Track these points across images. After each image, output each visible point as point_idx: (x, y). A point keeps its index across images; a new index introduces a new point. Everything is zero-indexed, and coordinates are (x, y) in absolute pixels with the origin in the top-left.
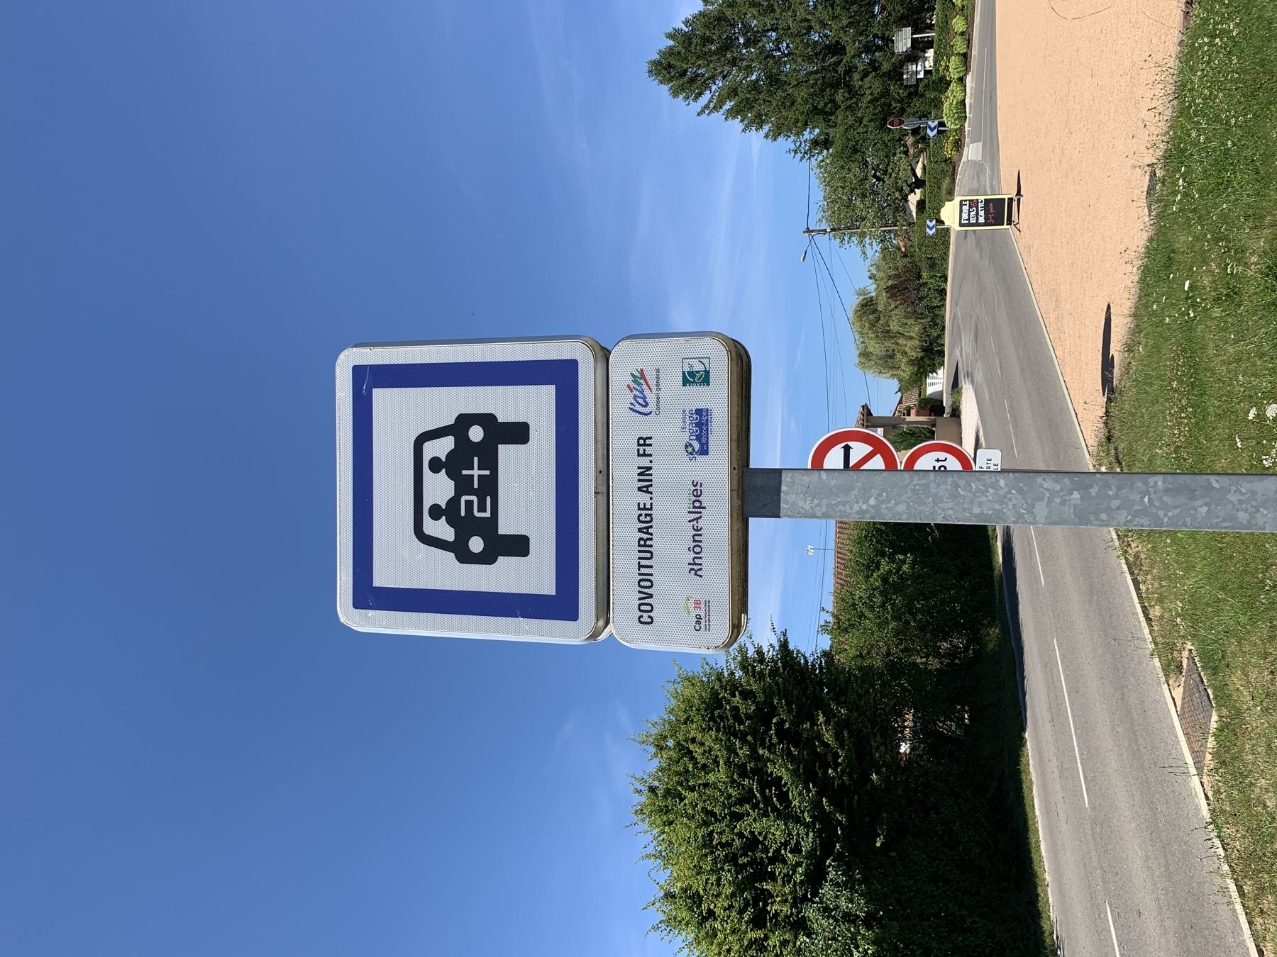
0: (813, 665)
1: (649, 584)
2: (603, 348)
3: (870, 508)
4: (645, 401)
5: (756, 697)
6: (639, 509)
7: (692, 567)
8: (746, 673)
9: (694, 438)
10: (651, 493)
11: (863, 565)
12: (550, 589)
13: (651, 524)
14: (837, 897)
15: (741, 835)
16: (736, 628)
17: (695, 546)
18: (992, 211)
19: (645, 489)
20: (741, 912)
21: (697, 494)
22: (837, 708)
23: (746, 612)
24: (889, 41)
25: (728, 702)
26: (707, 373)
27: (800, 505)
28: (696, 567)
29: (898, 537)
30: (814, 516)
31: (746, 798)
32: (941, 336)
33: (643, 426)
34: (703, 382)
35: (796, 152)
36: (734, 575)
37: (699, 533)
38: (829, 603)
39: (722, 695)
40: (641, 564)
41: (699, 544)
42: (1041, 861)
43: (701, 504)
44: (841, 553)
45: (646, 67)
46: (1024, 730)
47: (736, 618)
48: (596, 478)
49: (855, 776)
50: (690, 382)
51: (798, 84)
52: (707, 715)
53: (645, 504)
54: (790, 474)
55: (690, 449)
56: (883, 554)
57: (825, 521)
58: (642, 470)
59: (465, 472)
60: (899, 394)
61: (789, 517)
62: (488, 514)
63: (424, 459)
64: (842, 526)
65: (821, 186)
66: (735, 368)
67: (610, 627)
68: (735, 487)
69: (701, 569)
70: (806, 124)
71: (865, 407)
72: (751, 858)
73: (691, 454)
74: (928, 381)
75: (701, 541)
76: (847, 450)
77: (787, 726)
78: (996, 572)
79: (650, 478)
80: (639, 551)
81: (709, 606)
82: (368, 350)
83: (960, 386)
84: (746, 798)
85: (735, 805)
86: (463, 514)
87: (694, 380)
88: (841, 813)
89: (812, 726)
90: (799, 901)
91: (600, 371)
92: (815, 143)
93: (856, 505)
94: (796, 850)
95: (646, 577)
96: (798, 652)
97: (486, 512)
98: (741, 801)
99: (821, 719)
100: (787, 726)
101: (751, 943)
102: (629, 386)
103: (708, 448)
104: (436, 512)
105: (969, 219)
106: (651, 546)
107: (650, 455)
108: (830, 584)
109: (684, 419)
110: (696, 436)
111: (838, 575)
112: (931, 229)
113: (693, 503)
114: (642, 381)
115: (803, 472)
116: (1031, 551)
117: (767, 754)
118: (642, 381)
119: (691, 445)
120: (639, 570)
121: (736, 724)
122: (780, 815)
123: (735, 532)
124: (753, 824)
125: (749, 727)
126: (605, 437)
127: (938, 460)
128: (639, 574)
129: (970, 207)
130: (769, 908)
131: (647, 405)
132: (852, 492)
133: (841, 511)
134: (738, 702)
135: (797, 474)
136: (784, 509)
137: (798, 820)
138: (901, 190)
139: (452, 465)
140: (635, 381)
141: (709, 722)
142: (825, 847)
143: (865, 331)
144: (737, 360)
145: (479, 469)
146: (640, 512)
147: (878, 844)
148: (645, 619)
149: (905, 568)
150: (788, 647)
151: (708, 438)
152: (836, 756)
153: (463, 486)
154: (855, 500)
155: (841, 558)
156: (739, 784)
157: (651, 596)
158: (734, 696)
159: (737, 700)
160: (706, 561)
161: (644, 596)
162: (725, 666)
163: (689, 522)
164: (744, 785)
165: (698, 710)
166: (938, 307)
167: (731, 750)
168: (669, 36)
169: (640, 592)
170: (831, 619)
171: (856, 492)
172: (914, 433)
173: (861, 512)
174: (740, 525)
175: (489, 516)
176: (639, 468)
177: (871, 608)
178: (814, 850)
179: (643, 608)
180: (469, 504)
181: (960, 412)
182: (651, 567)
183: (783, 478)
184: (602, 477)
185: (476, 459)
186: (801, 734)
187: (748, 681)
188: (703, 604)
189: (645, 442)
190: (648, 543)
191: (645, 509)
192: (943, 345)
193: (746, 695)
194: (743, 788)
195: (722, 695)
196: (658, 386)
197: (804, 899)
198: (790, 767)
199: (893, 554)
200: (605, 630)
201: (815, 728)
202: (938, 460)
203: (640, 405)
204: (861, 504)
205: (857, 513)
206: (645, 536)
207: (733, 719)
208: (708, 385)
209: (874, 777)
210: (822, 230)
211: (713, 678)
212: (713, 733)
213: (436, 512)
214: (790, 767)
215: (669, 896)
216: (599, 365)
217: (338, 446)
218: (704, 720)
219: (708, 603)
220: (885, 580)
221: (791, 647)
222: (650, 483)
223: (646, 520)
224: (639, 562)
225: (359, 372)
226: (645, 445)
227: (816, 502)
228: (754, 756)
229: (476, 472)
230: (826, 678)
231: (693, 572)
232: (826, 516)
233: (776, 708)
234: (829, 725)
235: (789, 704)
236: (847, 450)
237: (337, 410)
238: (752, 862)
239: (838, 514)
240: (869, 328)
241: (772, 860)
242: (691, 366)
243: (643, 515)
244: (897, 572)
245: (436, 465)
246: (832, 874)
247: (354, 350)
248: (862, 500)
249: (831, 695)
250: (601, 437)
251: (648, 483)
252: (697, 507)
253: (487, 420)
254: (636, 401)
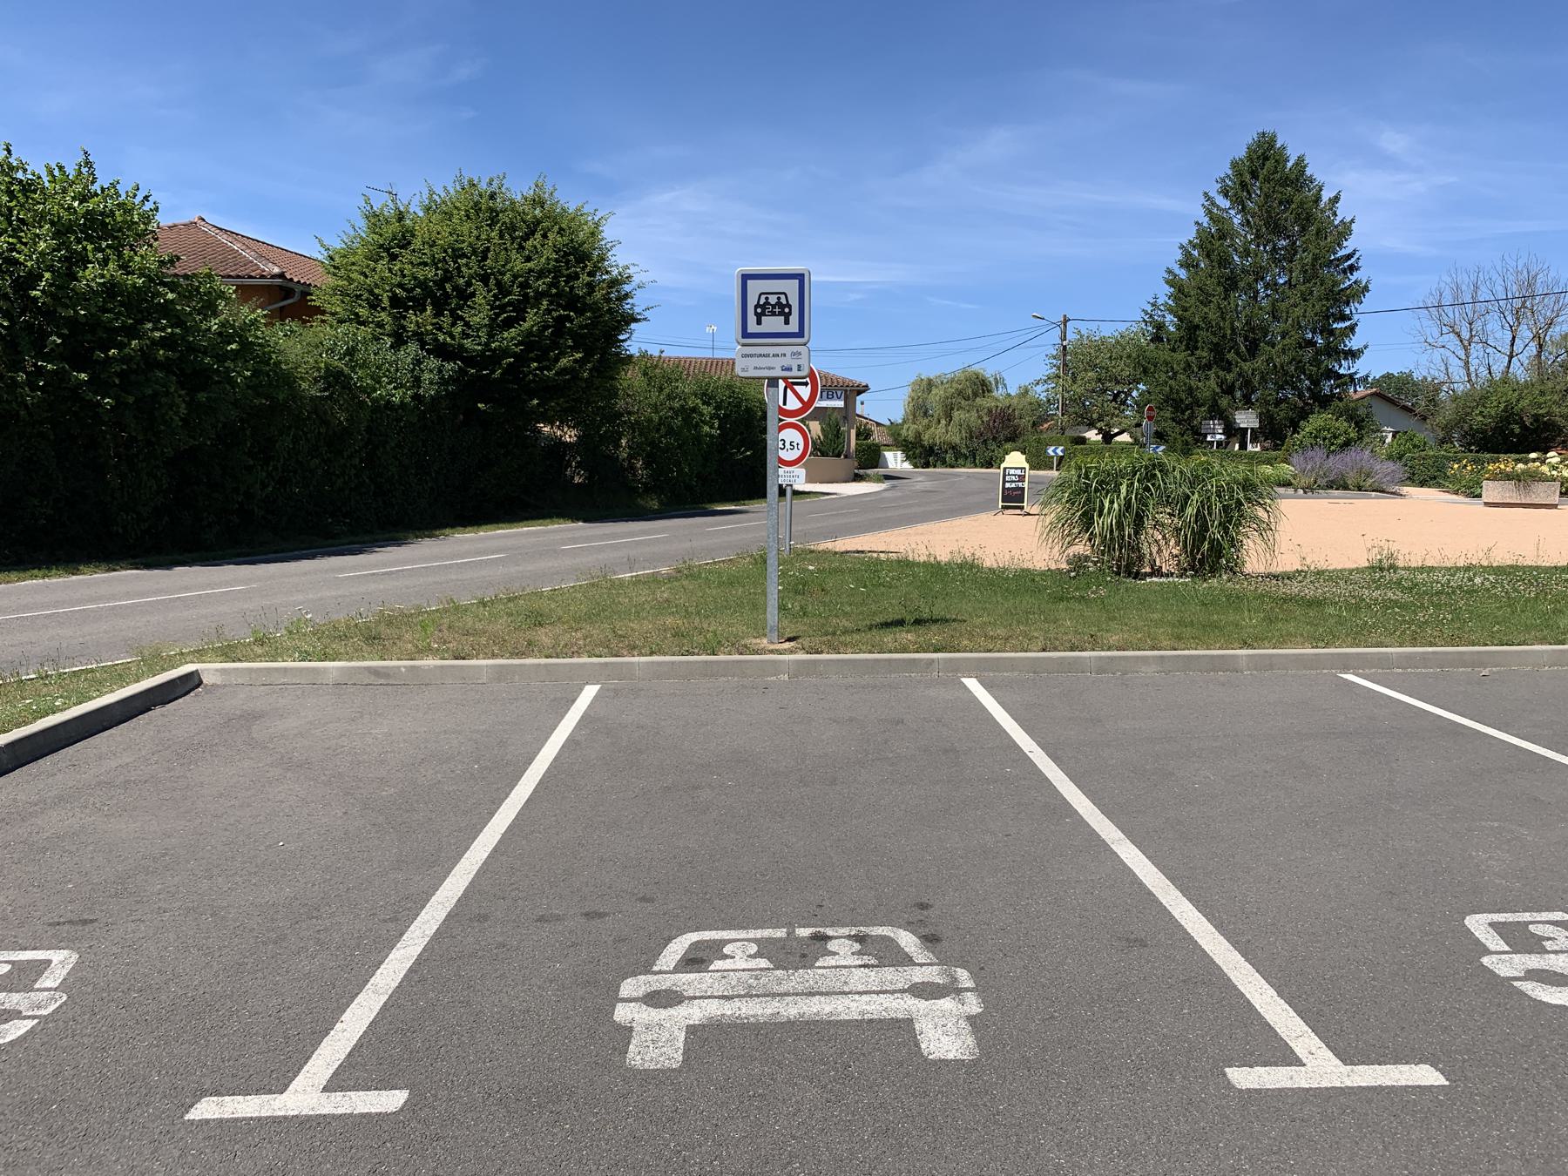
11: (707, 390)
14: (431, 371)
15: (469, 284)
18: (1014, 493)
19: (773, 356)
20: (400, 285)
24: (1248, 403)
29: (735, 422)
31: (503, 290)
32: (944, 464)
33: (788, 355)
35: (1153, 305)
42: (491, 530)
44: (712, 365)
45: (1269, 130)
46: (585, 521)
49: (532, 385)
51: (1220, 308)
56: (718, 408)
60: (888, 423)
65: (1116, 334)
70: (1180, 319)
71: (865, 389)
72: (452, 294)
74: (899, 453)
78: (707, 506)
83: (886, 481)
84: (503, 290)
85: (496, 279)
88: (501, 374)
89: (570, 347)
90: (419, 337)
92: (1160, 327)
94: (465, 335)
98: (499, 284)
99: (579, 356)
101: (377, 297)
104: (767, 299)
105: (1009, 475)
112: (1054, 451)
116: (731, 524)
117: (543, 307)
122: (493, 320)
124: (482, 295)
125: (564, 290)
127: (798, 444)
129: (1019, 476)
130: (411, 312)
137: (491, 336)
138: (1100, 419)
139: (779, 303)
142: (470, 361)
143: (954, 385)
147: (479, 405)
149: (706, 429)
152: (549, 369)
153: (774, 307)
155: (712, 365)
156: (513, 282)
160: (758, 371)
164: (513, 286)
166: (975, 459)
167: (541, 274)
168: (1300, 160)
172: (838, 438)
177: (669, 397)
178: (466, 350)
181: (859, 481)
186: (562, 338)
192: (935, 467)
193: (591, 287)
194: (511, 286)
197: (423, 345)
198: (535, 329)
199: (718, 417)
202: (798, 444)
203: (794, 354)
209: (536, 402)
210: (1065, 336)
212: (554, 256)
213: (767, 299)
214: (535, 329)
215: (401, 217)
220: (694, 410)
221: (633, 326)
228: (540, 295)
236: (806, 384)
238: (447, 296)
241: (452, 312)
244: (702, 421)
245: (779, 298)
246: (449, 366)
252: (770, 368)
253: (790, 313)
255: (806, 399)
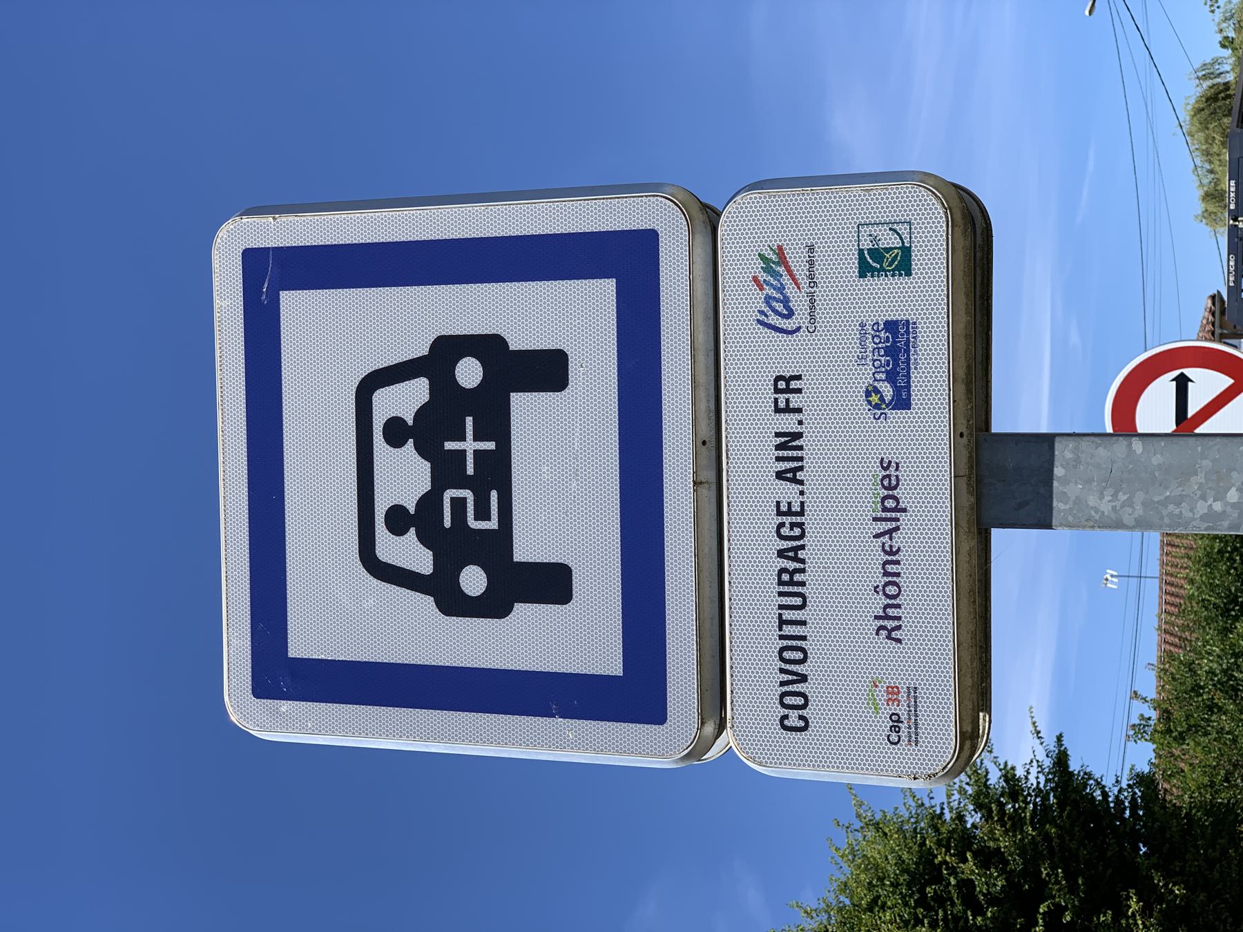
0: (1118, 801)
1: (799, 655)
2: (705, 207)
3: (1229, 509)
4: (787, 307)
5: (1006, 863)
6: (780, 513)
7: (881, 623)
8: (988, 817)
9: (883, 376)
10: (801, 483)
11: (1216, 606)
12: (612, 664)
13: (801, 542)
16: (970, 737)
17: (887, 584)
19: (789, 476)
21: (890, 485)
22: (1166, 885)
23: (987, 709)
25: (953, 871)
26: (906, 252)
27: (1091, 504)
28: (890, 624)
30: (1118, 525)
34: (897, 268)
36: (962, 639)
37: (894, 558)
38: (1149, 685)
39: (940, 858)
40: (784, 617)
41: (895, 579)
43: (898, 503)
44: (1171, 584)
47: (968, 720)
48: (696, 455)
50: (872, 270)
52: (911, 896)
53: (789, 504)
54: (1071, 444)
55: (875, 399)
57: (1140, 533)
58: (783, 440)
59: (449, 446)
61: (1070, 526)
62: (493, 524)
63: (375, 417)
64: (1169, 542)
66: (961, 242)
67: (727, 737)
68: (964, 470)
69: (899, 628)
73: (877, 407)
75: (898, 575)
76: (1182, 384)
77: (1068, 918)
79: (799, 453)
80: (781, 594)
81: (916, 698)
82: (271, 219)
86: (447, 523)
87: (881, 266)
89: (1116, 919)
91: (701, 253)
93: (1200, 503)
95: (794, 643)
96: (1089, 775)
97: (489, 519)
99: (1134, 905)
100: (1068, 918)
102: (755, 279)
103: (910, 395)
104: (398, 520)
106: (803, 584)
107: (799, 410)
108: (1150, 648)
109: (863, 335)
110: (887, 372)
111: (1165, 631)
113: (883, 502)
114: (781, 269)
115: (1097, 440)
118: (781, 269)
119: (876, 391)
120: (780, 629)
121: (969, 913)
123: (964, 557)
126: (712, 377)
128: (782, 637)
131: (790, 314)
132: (1194, 479)
133: (1171, 515)
134: (972, 872)
135: (1085, 444)
136: (1059, 511)
140: (768, 270)
141: (915, 908)
143: (1215, 149)
144: (965, 224)
145: (475, 440)
146: (781, 519)
148: (794, 721)
150: (1067, 766)
151: (909, 377)
154: (1199, 493)
155: (1172, 595)
157: (803, 678)
158: (965, 860)
159: (969, 867)
161: (790, 677)
162: (945, 801)
163: (874, 537)
165: (895, 885)
169: (782, 671)
170: (1154, 715)
171: (1200, 478)
173: (1210, 516)
174: (974, 543)
175: (496, 527)
176: (778, 435)
179: (789, 700)
180: (458, 504)
182: (803, 623)
183: (1056, 453)
184: (707, 454)
185: (469, 421)
187: (992, 831)
188: (903, 691)
189: (788, 385)
190: (797, 577)
191: (789, 513)
193: (988, 858)
195: (940, 858)
196: (811, 277)
200: (719, 741)
201: (1123, 922)
204: (1210, 501)
205: (1203, 518)
206: (792, 565)
207: (963, 904)
208: (909, 274)
211: (922, 825)
213: (398, 520)
216: (699, 239)
217: (219, 399)
218: (906, 904)
219: (913, 691)
221: (1074, 766)
222: (800, 464)
223: (792, 533)
224: (780, 615)
225: (254, 261)
226: (788, 390)
227: (1123, 497)
229: (470, 445)
230: (1145, 826)
231: (884, 633)
232: (1142, 524)
233: (1046, 883)
234: (1151, 916)
235: (1070, 877)
236: (1182, 384)
237: (217, 333)
239: (1167, 520)
240: (1223, 143)
242: (875, 239)
243: (787, 525)
245: (396, 432)
247: (245, 220)
248: (1214, 493)
249: (1154, 860)
250: (705, 378)
251: (795, 464)
254: (770, 307)
255: (1225, 382)
